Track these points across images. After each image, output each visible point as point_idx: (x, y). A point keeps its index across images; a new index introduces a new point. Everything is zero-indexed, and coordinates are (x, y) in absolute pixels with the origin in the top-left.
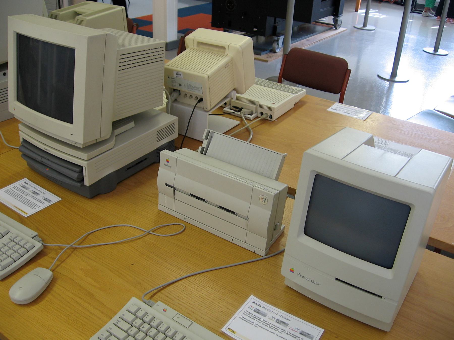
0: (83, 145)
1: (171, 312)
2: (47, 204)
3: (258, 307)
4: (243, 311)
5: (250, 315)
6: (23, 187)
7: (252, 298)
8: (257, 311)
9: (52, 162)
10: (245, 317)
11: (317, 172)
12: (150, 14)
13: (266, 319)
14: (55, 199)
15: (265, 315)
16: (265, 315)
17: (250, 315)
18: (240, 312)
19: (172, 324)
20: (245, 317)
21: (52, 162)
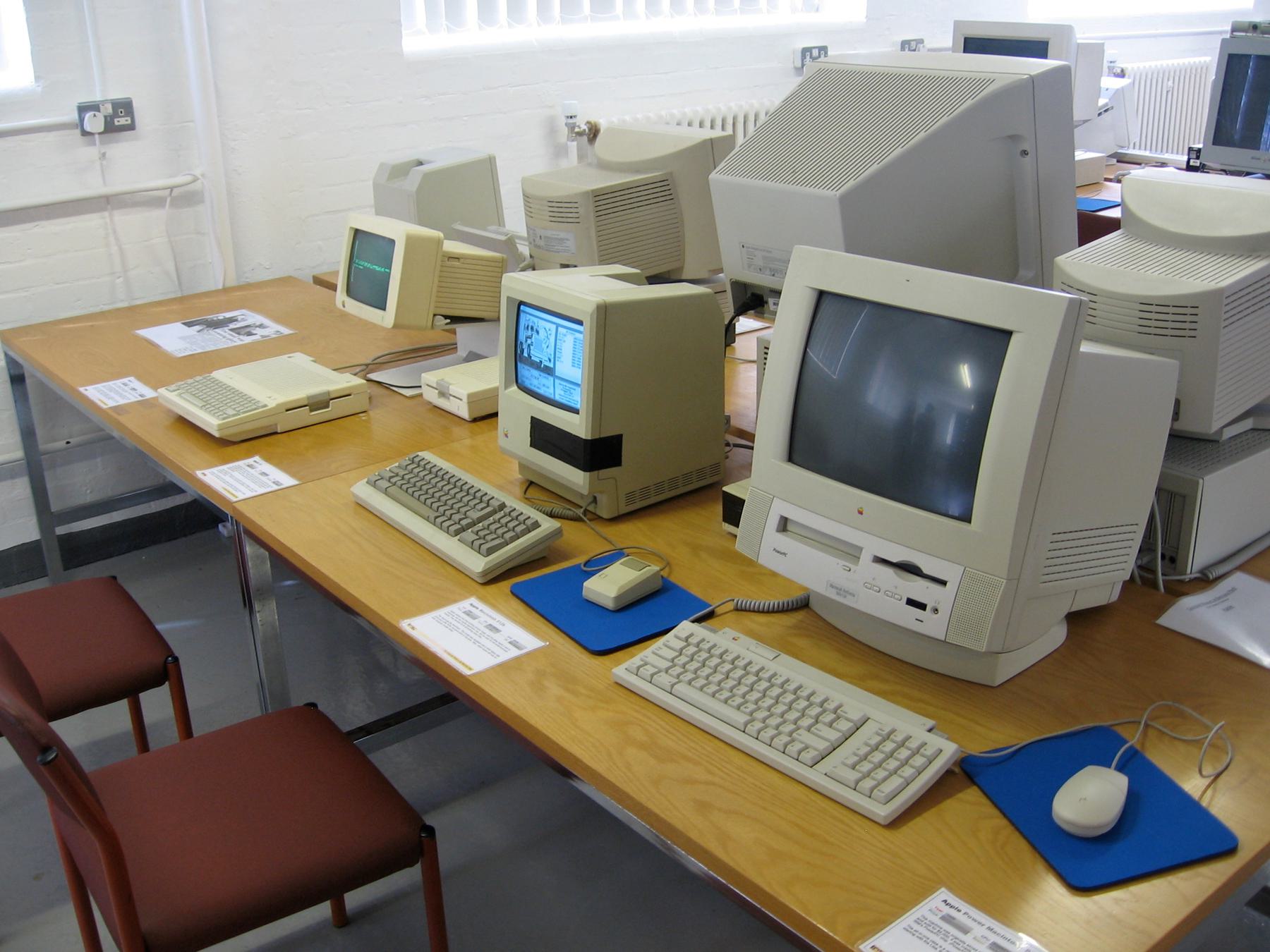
0: (617, 598)
1: (745, 639)
2: (514, 653)
3: (953, 913)
4: (914, 917)
5: (930, 926)
6: (468, 613)
7: (943, 894)
8: (948, 919)
9: (974, 920)
10: (916, 927)
11: (806, 589)
12: (482, 154)
13: (968, 939)
14: (531, 642)
15: (965, 931)
16: (965, 931)
17: (930, 926)
18: (909, 919)
19: (743, 652)
20: (916, 927)
21: (974, 920)
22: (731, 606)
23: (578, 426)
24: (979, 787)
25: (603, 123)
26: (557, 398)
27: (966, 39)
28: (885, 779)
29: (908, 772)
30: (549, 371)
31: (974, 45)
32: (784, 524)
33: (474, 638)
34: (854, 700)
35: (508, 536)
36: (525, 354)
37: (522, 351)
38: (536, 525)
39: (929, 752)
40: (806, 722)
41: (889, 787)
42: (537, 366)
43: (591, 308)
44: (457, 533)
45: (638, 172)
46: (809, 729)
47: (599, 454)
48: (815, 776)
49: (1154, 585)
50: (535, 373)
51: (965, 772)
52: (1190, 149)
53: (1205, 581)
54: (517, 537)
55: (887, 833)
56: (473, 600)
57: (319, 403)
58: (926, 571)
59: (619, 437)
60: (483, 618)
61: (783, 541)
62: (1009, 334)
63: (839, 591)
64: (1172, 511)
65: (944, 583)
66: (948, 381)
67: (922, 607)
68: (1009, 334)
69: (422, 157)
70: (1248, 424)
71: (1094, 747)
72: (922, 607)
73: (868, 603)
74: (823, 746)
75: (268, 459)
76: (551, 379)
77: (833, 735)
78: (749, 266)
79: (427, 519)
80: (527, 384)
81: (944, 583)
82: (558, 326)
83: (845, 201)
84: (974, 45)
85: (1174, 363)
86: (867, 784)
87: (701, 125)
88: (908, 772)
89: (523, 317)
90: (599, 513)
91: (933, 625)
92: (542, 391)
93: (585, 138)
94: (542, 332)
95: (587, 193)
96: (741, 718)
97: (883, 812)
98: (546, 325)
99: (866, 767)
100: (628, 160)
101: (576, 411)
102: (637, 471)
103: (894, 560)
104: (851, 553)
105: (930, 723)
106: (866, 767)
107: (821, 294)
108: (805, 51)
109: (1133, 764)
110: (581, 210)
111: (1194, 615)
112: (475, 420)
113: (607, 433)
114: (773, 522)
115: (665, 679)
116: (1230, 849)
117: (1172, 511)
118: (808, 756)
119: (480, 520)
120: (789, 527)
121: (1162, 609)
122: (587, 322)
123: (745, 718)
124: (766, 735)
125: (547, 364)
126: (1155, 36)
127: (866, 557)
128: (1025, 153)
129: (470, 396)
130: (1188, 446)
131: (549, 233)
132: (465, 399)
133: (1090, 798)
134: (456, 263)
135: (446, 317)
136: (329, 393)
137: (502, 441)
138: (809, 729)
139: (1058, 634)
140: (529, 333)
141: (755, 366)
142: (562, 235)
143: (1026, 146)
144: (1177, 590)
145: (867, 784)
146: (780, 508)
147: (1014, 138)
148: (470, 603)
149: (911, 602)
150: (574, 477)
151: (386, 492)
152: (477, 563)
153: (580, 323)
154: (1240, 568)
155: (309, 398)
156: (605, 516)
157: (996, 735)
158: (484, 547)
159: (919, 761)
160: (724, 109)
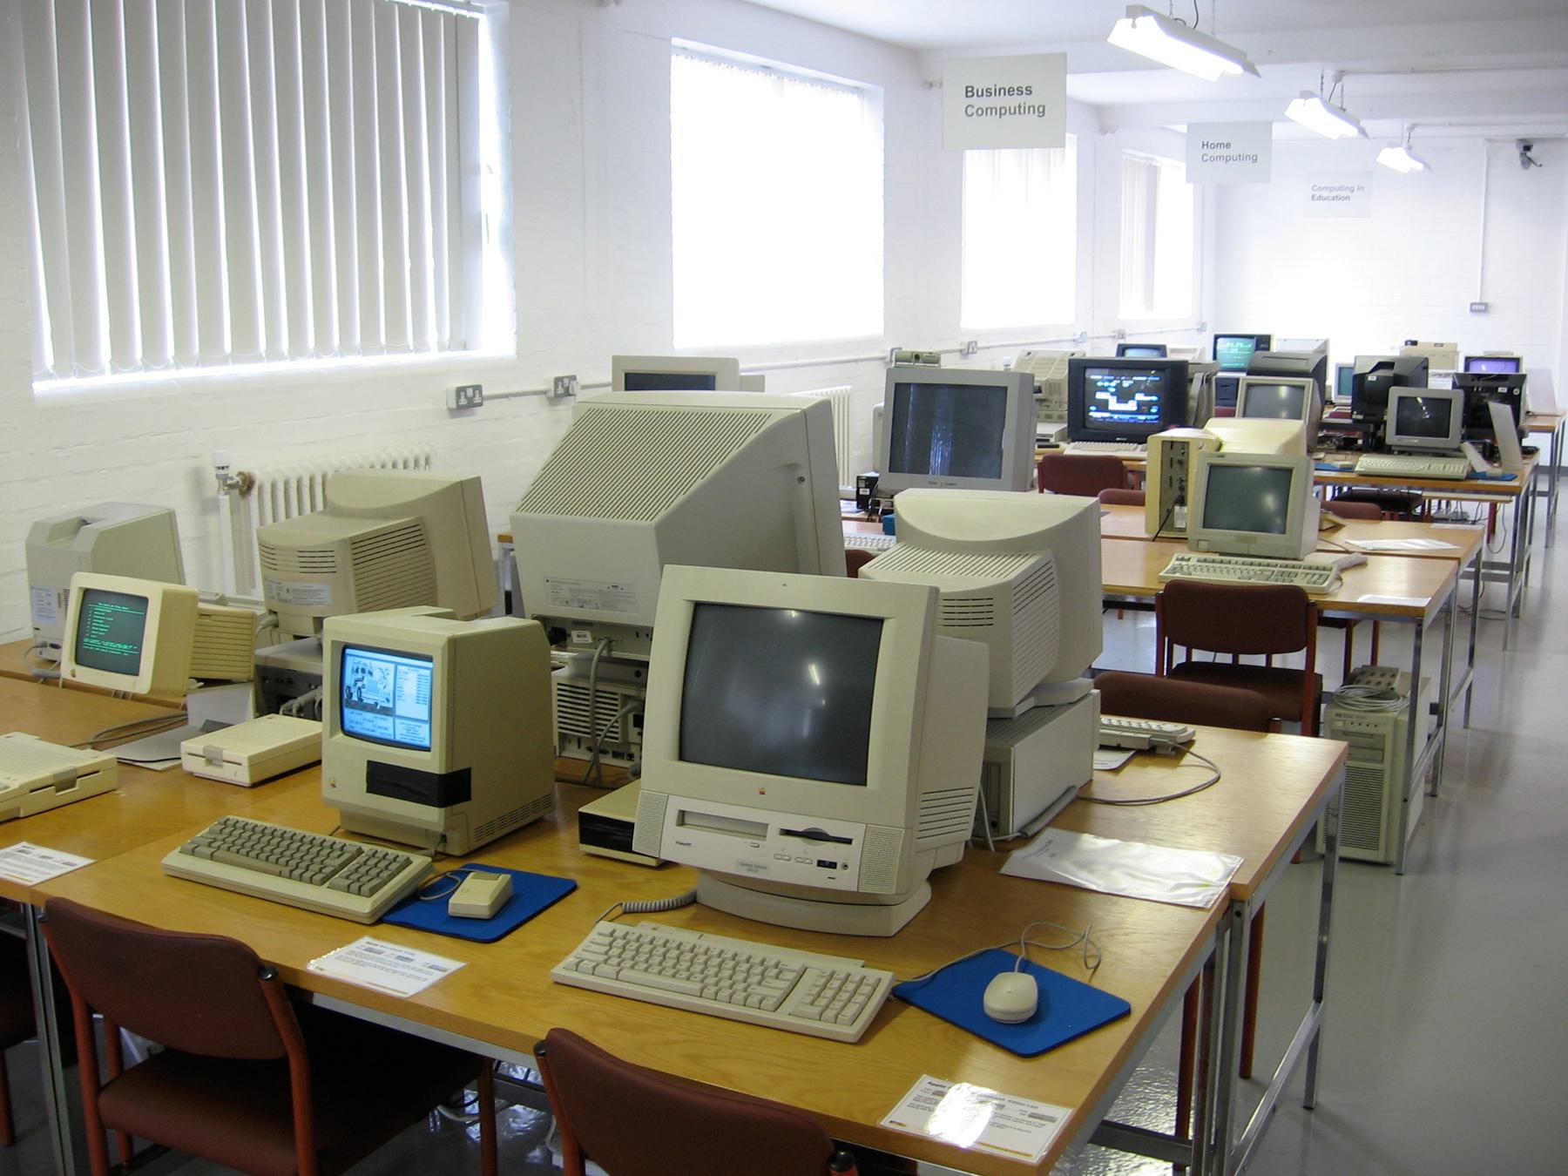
14: (453, 965)
22: (619, 910)
23: (432, 763)
24: (918, 1007)
25: (259, 477)
26: (398, 738)
27: (627, 375)
28: (843, 1008)
29: (860, 999)
30: (387, 712)
31: (636, 381)
32: (682, 818)
33: (389, 973)
34: (793, 958)
35: (385, 874)
36: (355, 698)
37: (351, 695)
38: (408, 862)
39: (872, 981)
40: (754, 979)
41: (851, 1010)
42: (372, 708)
43: (442, 642)
44: (323, 882)
45: (386, 517)
46: (759, 983)
47: (450, 789)
48: (781, 1017)
49: (985, 847)
50: (369, 715)
51: (900, 997)
52: (859, 478)
53: (1024, 838)
54: (385, 883)
55: (860, 1049)
56: (367, 939)
57: (65, 782)
58: (832, 834)
59: (469, 770)
60: (388, 952)
61: (686, 833)
62: (881, 621)
63: (749, 866)
64: (995, 775)
65: (849, 841)
66: (799, 680)
67: (833, 865)
68: (881, 621)
69: (85, 515)
70: (1031, 703)
71: (1001, 962)
72: (833, 865)
73: (779, 872)
74: (778, 993)
75: (39, 842)
76: (390, 719)
77: (785, 985)
78: (554, 600)
79: (280, 874)
80: (358, 729)
81: (849, 841)
82: (397, 664)
83: (659, 529)
84: (636, 381)
85: (985, 646)
86: (830, 1013)
87: (394, 466)
88: (860, 999)
89: (350, 663)
90: (449, 851)
91: (845, 881)
92: (377, 734)
93: (237, 491)
94: (377, 674)
95: (344, 541)
96: (697, 987)
97: (854, 1031)
98: (381, 667)
99: (822, 1002)
100: (375, 506)
101: (427, 749)
102: (523, 789)
103: (800, 829)
104: (759, 830)
105: (861, 962)
106: (822, 1002)
107: (698, 606)
108: (460, 391)
109: (1026, 967)
110: (338, 559)
111: (1021, 863)
112: (254, 786)
113: (459, 767)
114: (671, 817)
115: (604, 968)
116: (1126, 1013)
117: (995, 775)
118: (770, 1003)
119: (342, 866)
120: (687, 820)
121: (1001, 863)
122: (438, 658)
123: (699, 986)
124: (725, 993)
125: (385, 704)
126: (796, 366)
127: (773, 832)
128: (802, 479)
129: (251, 759)
130: (999, 722)
131: (299, 586)
132: (246, 763)
133: (1009, 993)
134: (207, 621)
135: (199, 680)
136: (75, 770)
137: (327, 792)
138: (759, 983)
139: (923, 894)
140: (360, 675)
141: (1103, 533)
142: (315, 587)
143: (803, 473)
144: (1005, 848)
145: (830, 1013)
146: (675, 805)
147: (792, 467)
148: (365, 941)
149: (821, 864)
150: (429, 816)
151: (212, 857)
152: (363, 906)
153: (429, 659)
154: (1048, 825)
155: (55, 776)
156: (457, 853)
157: (916, 969)
158: (365, 888)
159: (865, 989)
160: (417, 450)
